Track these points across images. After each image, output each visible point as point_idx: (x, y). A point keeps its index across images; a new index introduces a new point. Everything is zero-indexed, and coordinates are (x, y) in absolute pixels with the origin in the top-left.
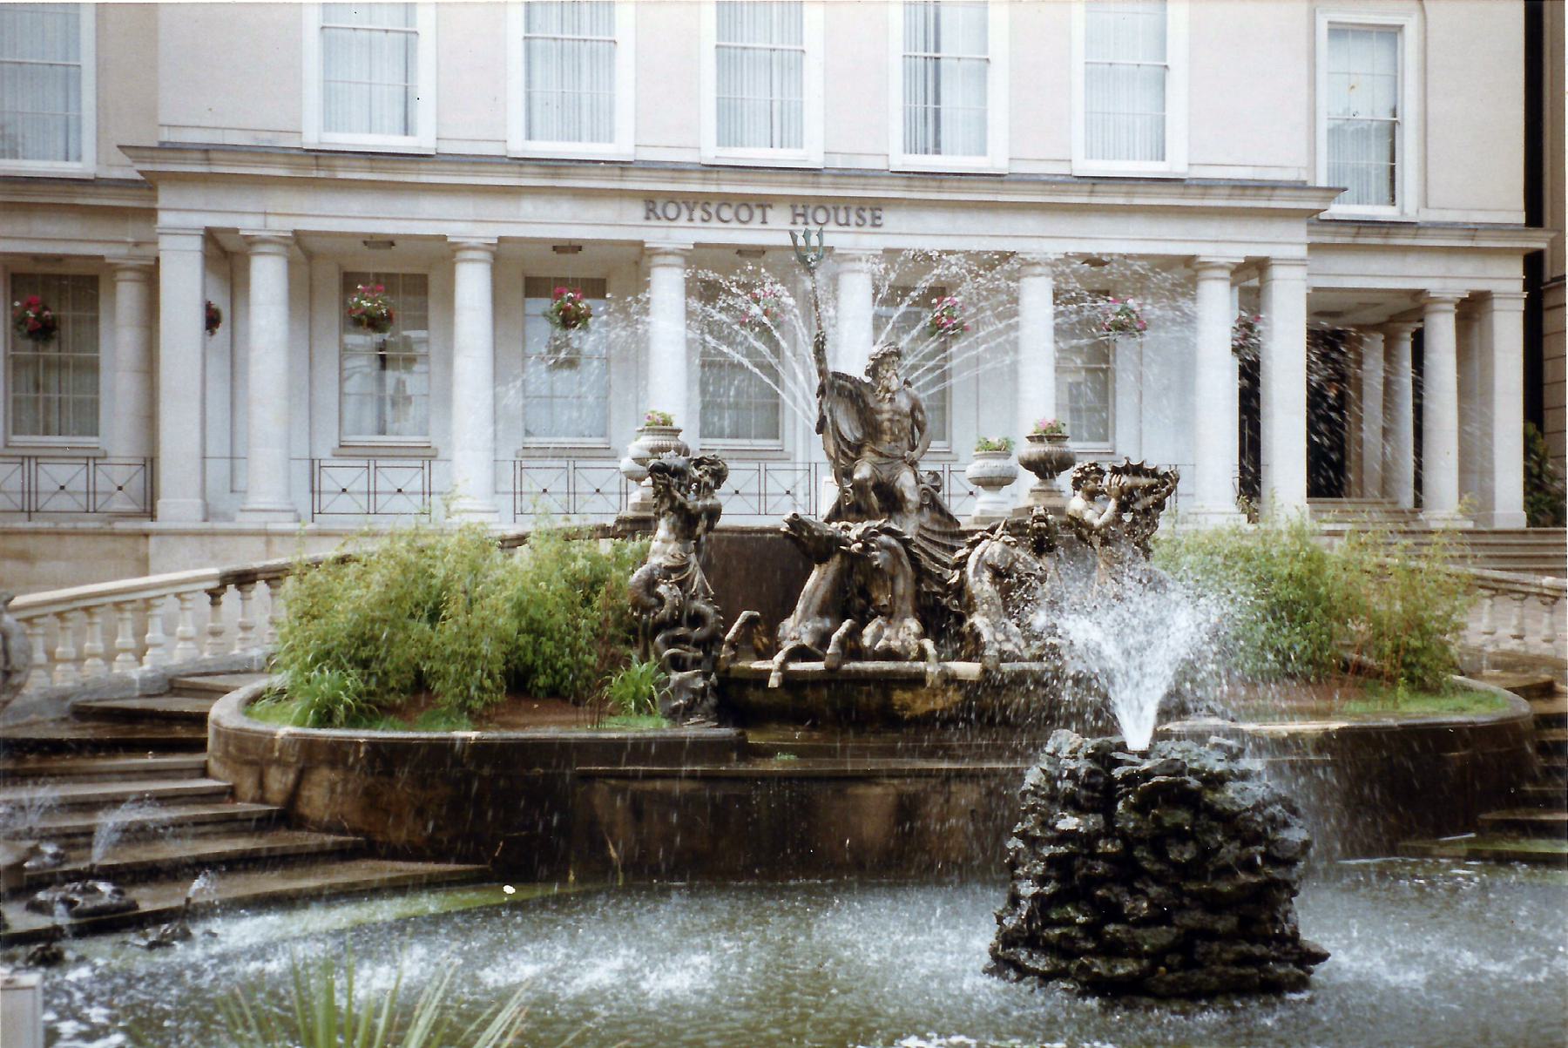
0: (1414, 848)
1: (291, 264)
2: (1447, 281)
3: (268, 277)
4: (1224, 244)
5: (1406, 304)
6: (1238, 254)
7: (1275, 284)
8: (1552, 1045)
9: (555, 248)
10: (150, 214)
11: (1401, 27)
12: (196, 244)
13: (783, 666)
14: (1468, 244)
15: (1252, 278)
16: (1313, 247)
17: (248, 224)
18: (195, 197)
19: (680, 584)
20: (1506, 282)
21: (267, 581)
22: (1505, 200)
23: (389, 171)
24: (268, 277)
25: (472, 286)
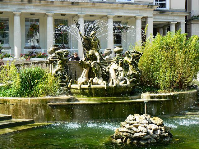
13: (80, 86)
19: (61, 72)
20: (183, 20)
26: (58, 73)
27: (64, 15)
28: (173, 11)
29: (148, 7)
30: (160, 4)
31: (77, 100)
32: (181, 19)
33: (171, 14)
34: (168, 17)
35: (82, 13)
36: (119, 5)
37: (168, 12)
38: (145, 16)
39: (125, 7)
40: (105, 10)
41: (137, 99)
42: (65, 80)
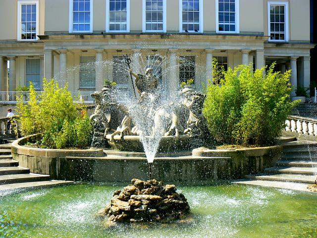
2: (294, 53)
21: (294, 120)
26: (95, 120)
27: (190, 51)
28: (293, 44)
29: (256, 38)
30: (277, 35)
31: (105, 155)
32: (305, 52)
33: (290, 47)
34: (288, 51)
35: (64, 47)
36: (219, 36)
37: (287, 45)
38: (254, 49)
39: (227, 39)
40: (202, 43)
41: (187, 155)
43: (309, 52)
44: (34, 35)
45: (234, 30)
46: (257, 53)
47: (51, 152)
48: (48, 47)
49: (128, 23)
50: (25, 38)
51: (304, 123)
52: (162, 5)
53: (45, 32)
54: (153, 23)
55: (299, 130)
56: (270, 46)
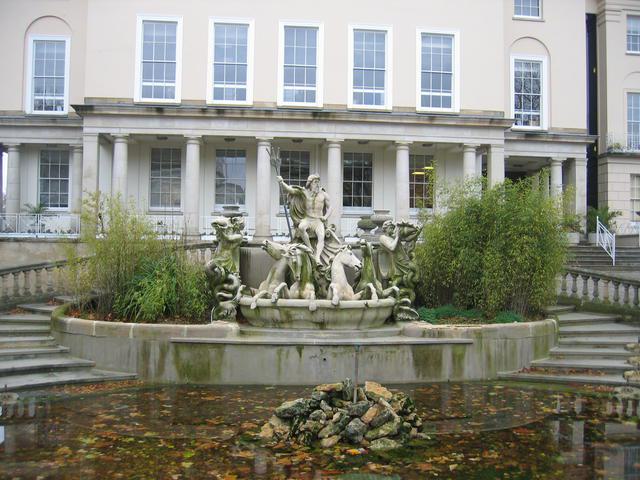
0: (434, 337)
1: (201, 147)
2: (558, 153)
3: (121, 149)
4: (472, 138)
5: (545, 162)
6: (479, 142)
7: (493, 155)
8: (198, 401)
9: (226, 139)
10: (81, 128)
11: (176, 23)
12: (96, 139)
14: (267, 117)
15: (483, 151)
16: (506, 140)
17: (113, 132)
18: (99, 122)
20: (580, 154)
21: (593, 278)
22: (582, 124)
23: (241, 114)
24: (121, 149)
25: (193, 153)
28: (555, 138)
42: (231, 287)
43: (585, 151)
44: (60, 104)
45: (314, 101)
46: (493, 149)
47: (139, 328)
48: (93, 127)
49: (178, 85)
50: (40, 108)
51: (590, 281)
52: (423, 48)
53: (393, 107)
54: (227, 86)
55: (580, 294)
56: (515, 138)
